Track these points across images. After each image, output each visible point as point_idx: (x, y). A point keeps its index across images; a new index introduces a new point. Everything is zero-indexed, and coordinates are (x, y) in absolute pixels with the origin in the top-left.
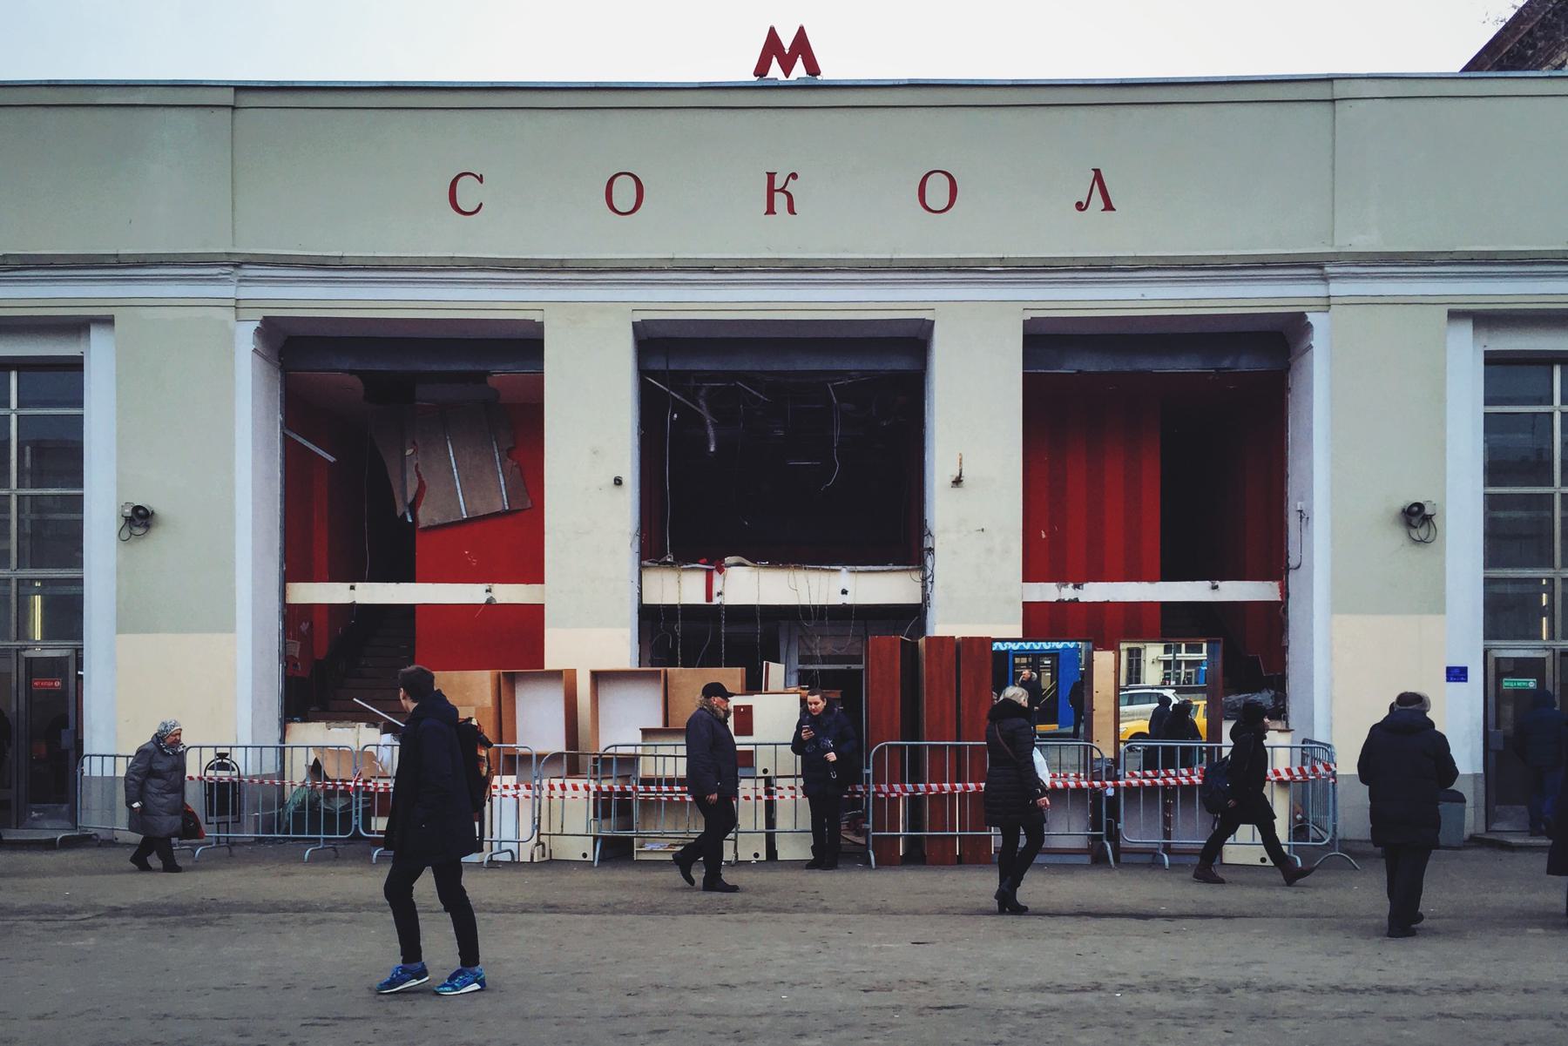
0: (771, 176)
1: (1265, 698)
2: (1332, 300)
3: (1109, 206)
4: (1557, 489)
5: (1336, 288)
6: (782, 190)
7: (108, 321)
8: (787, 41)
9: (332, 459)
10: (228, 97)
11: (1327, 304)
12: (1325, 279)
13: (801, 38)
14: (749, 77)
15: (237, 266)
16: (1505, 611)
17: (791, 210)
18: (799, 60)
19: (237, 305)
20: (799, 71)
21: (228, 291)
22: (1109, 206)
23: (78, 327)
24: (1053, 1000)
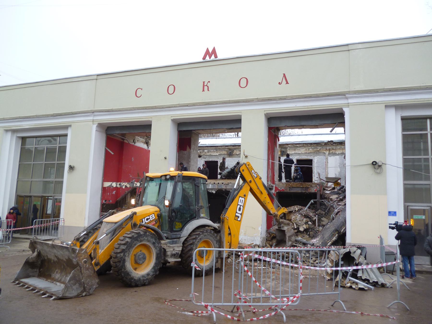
0: (204, 82)
1: (354, 272)
2: (349, 104)
3: (287, 83)
4: (430, 157)
5: (350, 101)
6: (206, 85)
7: (70, 126)
8: (210, 51)
9: (113, 153)
10: (95, 77)
11: (348, 105)
12: (347, 98)
13: (214, 50)
14: (202, 60)
15: (93, 112)
16: (410, 194)
17: (208, 90)
18: (213, 55)
19: (93, 121)
20: (213, 57)
21: (91, 118)
22: (287, 83)
23: (66, 127)
24: (283, 175)
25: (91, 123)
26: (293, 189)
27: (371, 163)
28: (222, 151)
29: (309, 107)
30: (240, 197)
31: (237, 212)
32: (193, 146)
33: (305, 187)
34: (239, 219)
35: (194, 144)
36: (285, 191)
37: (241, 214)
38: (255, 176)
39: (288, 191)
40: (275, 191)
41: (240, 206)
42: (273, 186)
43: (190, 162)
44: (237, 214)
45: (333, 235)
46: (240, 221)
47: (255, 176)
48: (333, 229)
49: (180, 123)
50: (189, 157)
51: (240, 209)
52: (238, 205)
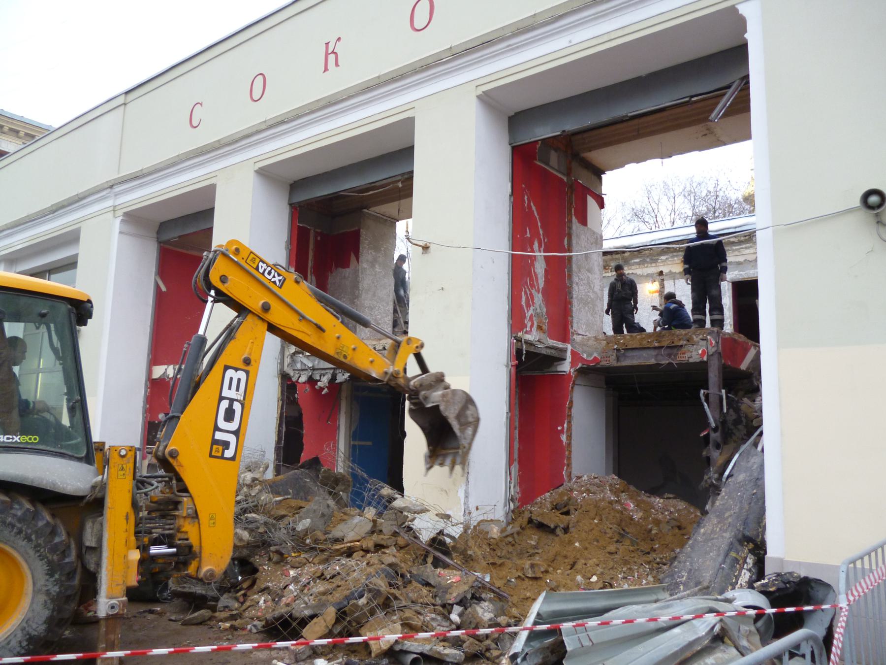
6: (333, 52)
10: (121, 100)
15: (111, 187)
17: (337, 65)
21: (109, 203)
25: (110, 215)
26: (630, 354)
27: (857, 202)
28: (578, 291)
29: (613, 36)
30: (227, 368)
31: (217, 428)
32: (366, 254)
33: (665, 344)
34: (229, 453)
35: (377, 249)
36: (604, 363)
37: (236, 433)
39: (612, 362)
40: (573, 364)
41: (232, 401)
42: (564, 351)
43: (357, 297)
44: (219, 436)
45: (736, 560)
46: (233, 459)
47: (277, 279)
49: (295, 182)
50: (355, 285)
51: (229, 416)
52: (221, 398)
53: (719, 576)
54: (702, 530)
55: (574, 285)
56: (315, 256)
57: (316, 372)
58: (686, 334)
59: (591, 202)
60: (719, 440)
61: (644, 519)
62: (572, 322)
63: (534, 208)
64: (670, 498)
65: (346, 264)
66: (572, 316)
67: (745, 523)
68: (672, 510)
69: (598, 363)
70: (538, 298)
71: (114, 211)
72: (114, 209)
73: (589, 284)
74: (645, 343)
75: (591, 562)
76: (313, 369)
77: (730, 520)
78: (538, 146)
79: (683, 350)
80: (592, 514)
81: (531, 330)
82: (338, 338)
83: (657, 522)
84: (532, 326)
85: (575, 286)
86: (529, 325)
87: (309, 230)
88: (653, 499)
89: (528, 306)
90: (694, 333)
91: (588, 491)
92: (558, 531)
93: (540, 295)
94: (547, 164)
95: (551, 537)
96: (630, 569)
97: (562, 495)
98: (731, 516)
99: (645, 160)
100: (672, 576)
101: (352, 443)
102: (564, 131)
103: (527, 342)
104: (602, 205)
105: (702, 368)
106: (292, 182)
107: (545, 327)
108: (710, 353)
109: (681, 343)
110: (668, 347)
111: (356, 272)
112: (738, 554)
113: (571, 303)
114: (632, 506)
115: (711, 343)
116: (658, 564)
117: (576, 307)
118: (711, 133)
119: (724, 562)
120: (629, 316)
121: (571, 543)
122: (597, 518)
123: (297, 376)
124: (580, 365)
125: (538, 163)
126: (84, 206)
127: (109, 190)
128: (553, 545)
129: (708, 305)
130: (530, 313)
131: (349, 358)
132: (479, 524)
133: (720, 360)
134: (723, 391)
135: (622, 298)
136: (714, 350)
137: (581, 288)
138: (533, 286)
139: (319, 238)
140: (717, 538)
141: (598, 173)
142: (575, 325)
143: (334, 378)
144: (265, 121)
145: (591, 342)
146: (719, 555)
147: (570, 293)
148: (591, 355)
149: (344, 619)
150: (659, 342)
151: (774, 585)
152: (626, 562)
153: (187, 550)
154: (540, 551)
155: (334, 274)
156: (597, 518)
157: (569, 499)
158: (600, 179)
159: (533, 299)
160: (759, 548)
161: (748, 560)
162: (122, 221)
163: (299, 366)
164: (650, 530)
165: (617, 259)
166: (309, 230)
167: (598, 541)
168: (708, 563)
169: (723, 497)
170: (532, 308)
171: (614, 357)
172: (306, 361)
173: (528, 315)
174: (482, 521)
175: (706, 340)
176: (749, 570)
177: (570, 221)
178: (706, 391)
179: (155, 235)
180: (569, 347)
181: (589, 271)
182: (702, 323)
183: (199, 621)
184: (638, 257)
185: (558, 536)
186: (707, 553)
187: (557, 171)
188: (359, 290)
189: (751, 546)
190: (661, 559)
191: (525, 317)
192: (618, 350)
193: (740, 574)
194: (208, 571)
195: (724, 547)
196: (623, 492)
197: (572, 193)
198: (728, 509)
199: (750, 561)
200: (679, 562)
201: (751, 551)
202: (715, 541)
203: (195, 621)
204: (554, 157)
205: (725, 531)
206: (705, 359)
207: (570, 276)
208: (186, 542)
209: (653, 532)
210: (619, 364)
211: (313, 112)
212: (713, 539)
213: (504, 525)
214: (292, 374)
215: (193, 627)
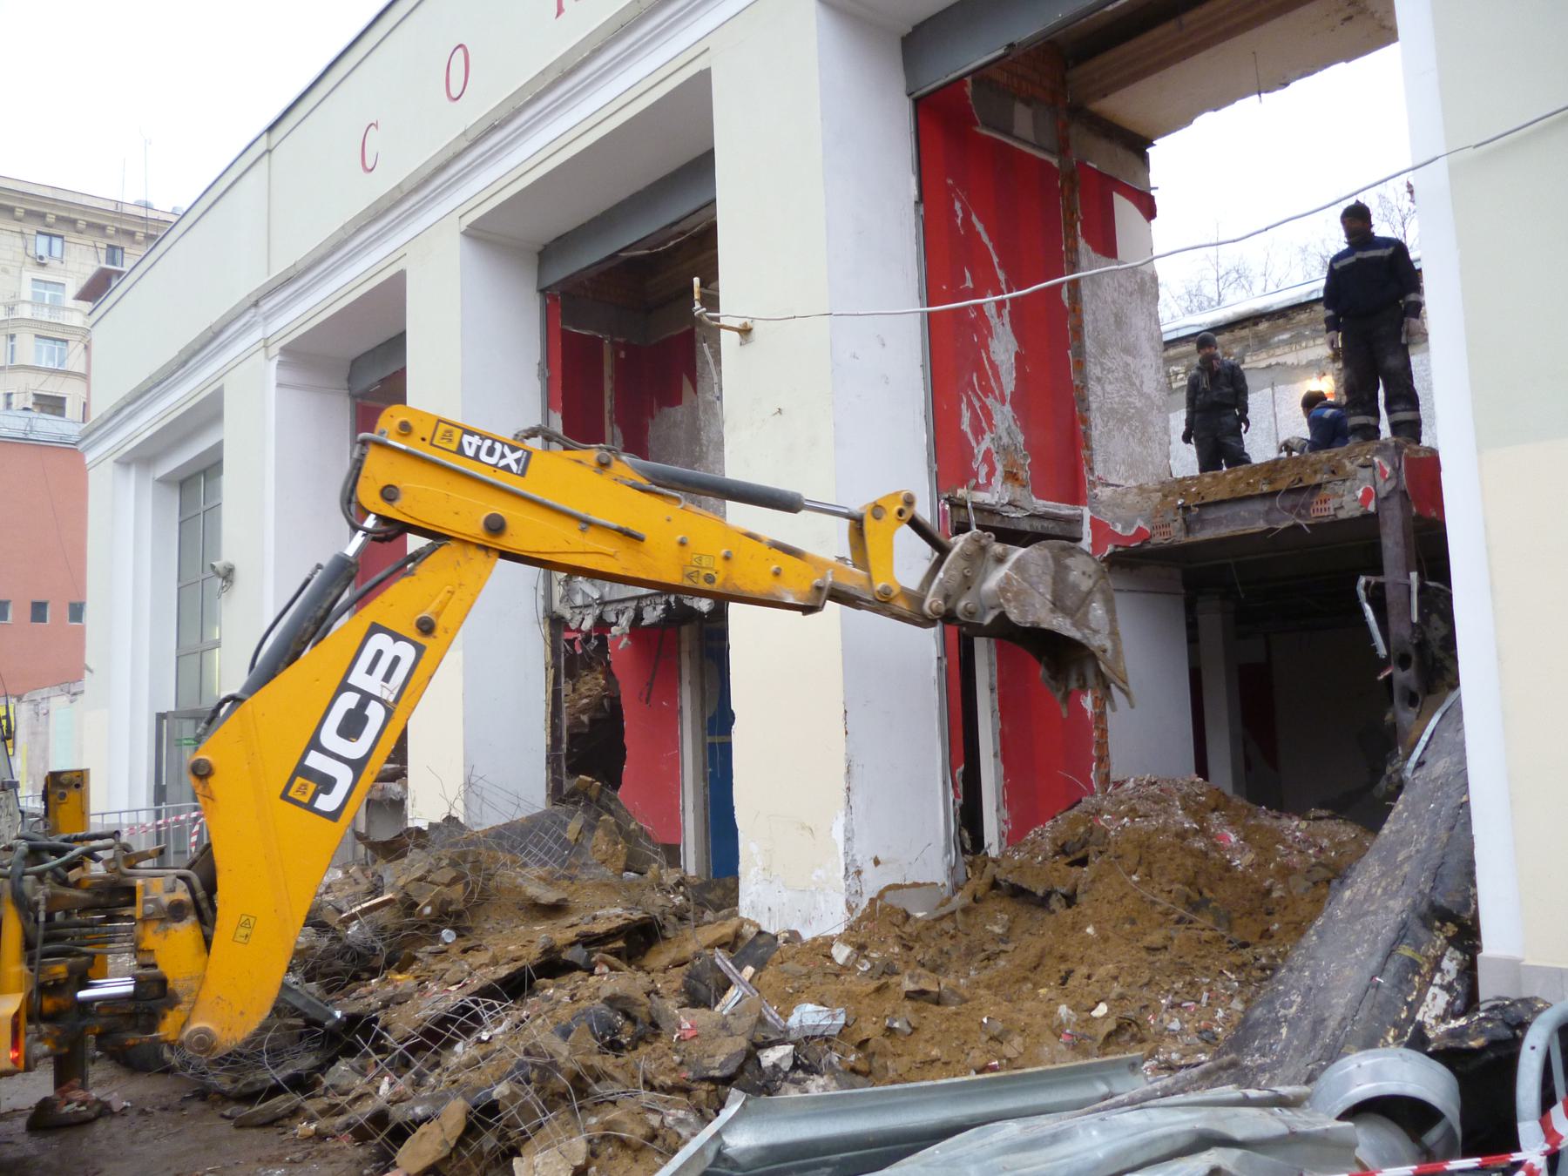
15: (256, 304)
21: (257, 335)
26: (1211, 514)
30: (375, 629)
31: (315, 744)
33: (1282, 485)
36: (1158, 539)
38: (511, 459)
41: (366, 698)
44: (315, 760)
45: (1414, 966)
47: (511, 459)
48: (1398, 906)
49: (546, 246)
50: (694, 434)
52: (344, 687)
53: (1367, 1004)
54: (1347, 894)
55: (1092, 384)
56: (617, 389)
57: (609, 608)
58: (1329, 459)
59: (1124, 208)
60: (1414, 685)
61: (1258, 866)
62: (1090, 461)
63: (980, 227)
64: (1321, 818)
65: (674, 399)
66: (1089, 448)
67: (1436, 876)
68: (1325, 843)
69: (1146, 541)
70: (1003, 416)
71: (266, 347)
72: (266, 344)
73: (1128, 378)
74: (1241, 489)
75: (1101, 972)
76: (603, 603)
77: (1406, 868)
78: (969, 90)
79: (1324, 493)
80: (1131, 860)
81: (989, 483)
82: (682, 543)
83: (1286, 872)
84: (991, 474)
85: (1093, 385)
86: (983, 471)
87: (602, 340)
88: (1285, 821)
89: (978, 432)
90: (1348, 456)
91: (1133, 812)
92: (1055, 903)
93: (1008, 408)
94: (1009, 133)
95: (1040, 914)
96: (1192, 984)
97: (1074, 823)
98: (1409, 858)
99: (1232, 101)
100: (1271, 1002)
101: (709, 739)
102: (1011, 46)
103: (979, 508)
104: (1149, 211)
105: (1368, 524)
106: (539, 248)
107: (1025, 474)
108: (1382, 494)
109: (1318, 479)
110: (1290, 491)
111: (695, 408)
112: (1417, 949)
113: (1085, 421)
114: (1233, 838)
115: (1383, 473)
116: (1263, 969)
117: (1098, 429)
118: (1363, 11)
119: (1381, 971)
120: (1230, 441)
121: (1077, 927)
122: (1141, 870)
123: (579, 618)
124: (1110, 548)
125: (985, 132)
126: (223, 346)
127: (253, 310)
128: (1039, 935)
129: (1381, 393)
130: (984, 446)
131: (719, 579)
132: (881, 895)
133: (1405, 507)
134: (1414, 575)
135: (1216, 405)
136: (1389, 486)
137: (1109, 388)
138: (987, 390)
139: (622, 355)
140: (1375, 913)
141: (1138, 145)
142: (1099, 470)
143: (638, 617)
144: (464, 133)
145: (1131, 499)
146: (1371, 955)
147: (1084, 400)
148: (1131, 525)
149: (488, 1127)
150: (1271, 483)
151: (1482, 1032)
152: (1183, 969)
153: (155, 989)
154: (1010, 947)
155: (657, 420)
156: (1141, 870)
157: (1090, 831)
158: (1144, 159)
159: (989, 416)
160: (1467, 936)
161: (1446, 964)
162: (280, 363)
163: (579, 600)
164: (1269, 891)
165: (1243, 339)
166: (602, 340)
167: (1133, 922)
168: (1347, 972)
169: (1400, 813)
170: (988, 436)
171: (1179, 524)
172: (588, 589)
173: (979, 450)
174: (889, 888)
175: (1371, 465)
176: (1448, 988)
177: (1074, 249)
178: (1373, 580)
179: (346, 385)
180: (1087, 513)
181: (1127, 350)
182: (1372, 432)
183: (266, 1120)
184: (1286, 330)
185: (1053, 912)
186: (1350, 948)
187: (1034, 146)
188: (701, 445)
189: (1451, 929)
190: (1273, 957)
191: (973, 456)
192: (1186, 508)
193: (1420, 999)
194: (199, 1031)
195: (1387, 933)
196: (1214, 810)
197: (1072, 191)
198: (1404, 844)
199: (1450, 965)
200: (1291, 970)
201: (1451, 941)
202: (1370, 918)
203: (259, 1120)
204: (1023, 119)
205: (1394, 896)
206: (1372, 508)
207: (1080, 364)
208: (151, 971)
209: (1276, 894)
210: (1191, 539)
211: (538, 97)
212: (1366, 914)
213: (946, 892)
214: (568, 616)
215: (254, 1131)
